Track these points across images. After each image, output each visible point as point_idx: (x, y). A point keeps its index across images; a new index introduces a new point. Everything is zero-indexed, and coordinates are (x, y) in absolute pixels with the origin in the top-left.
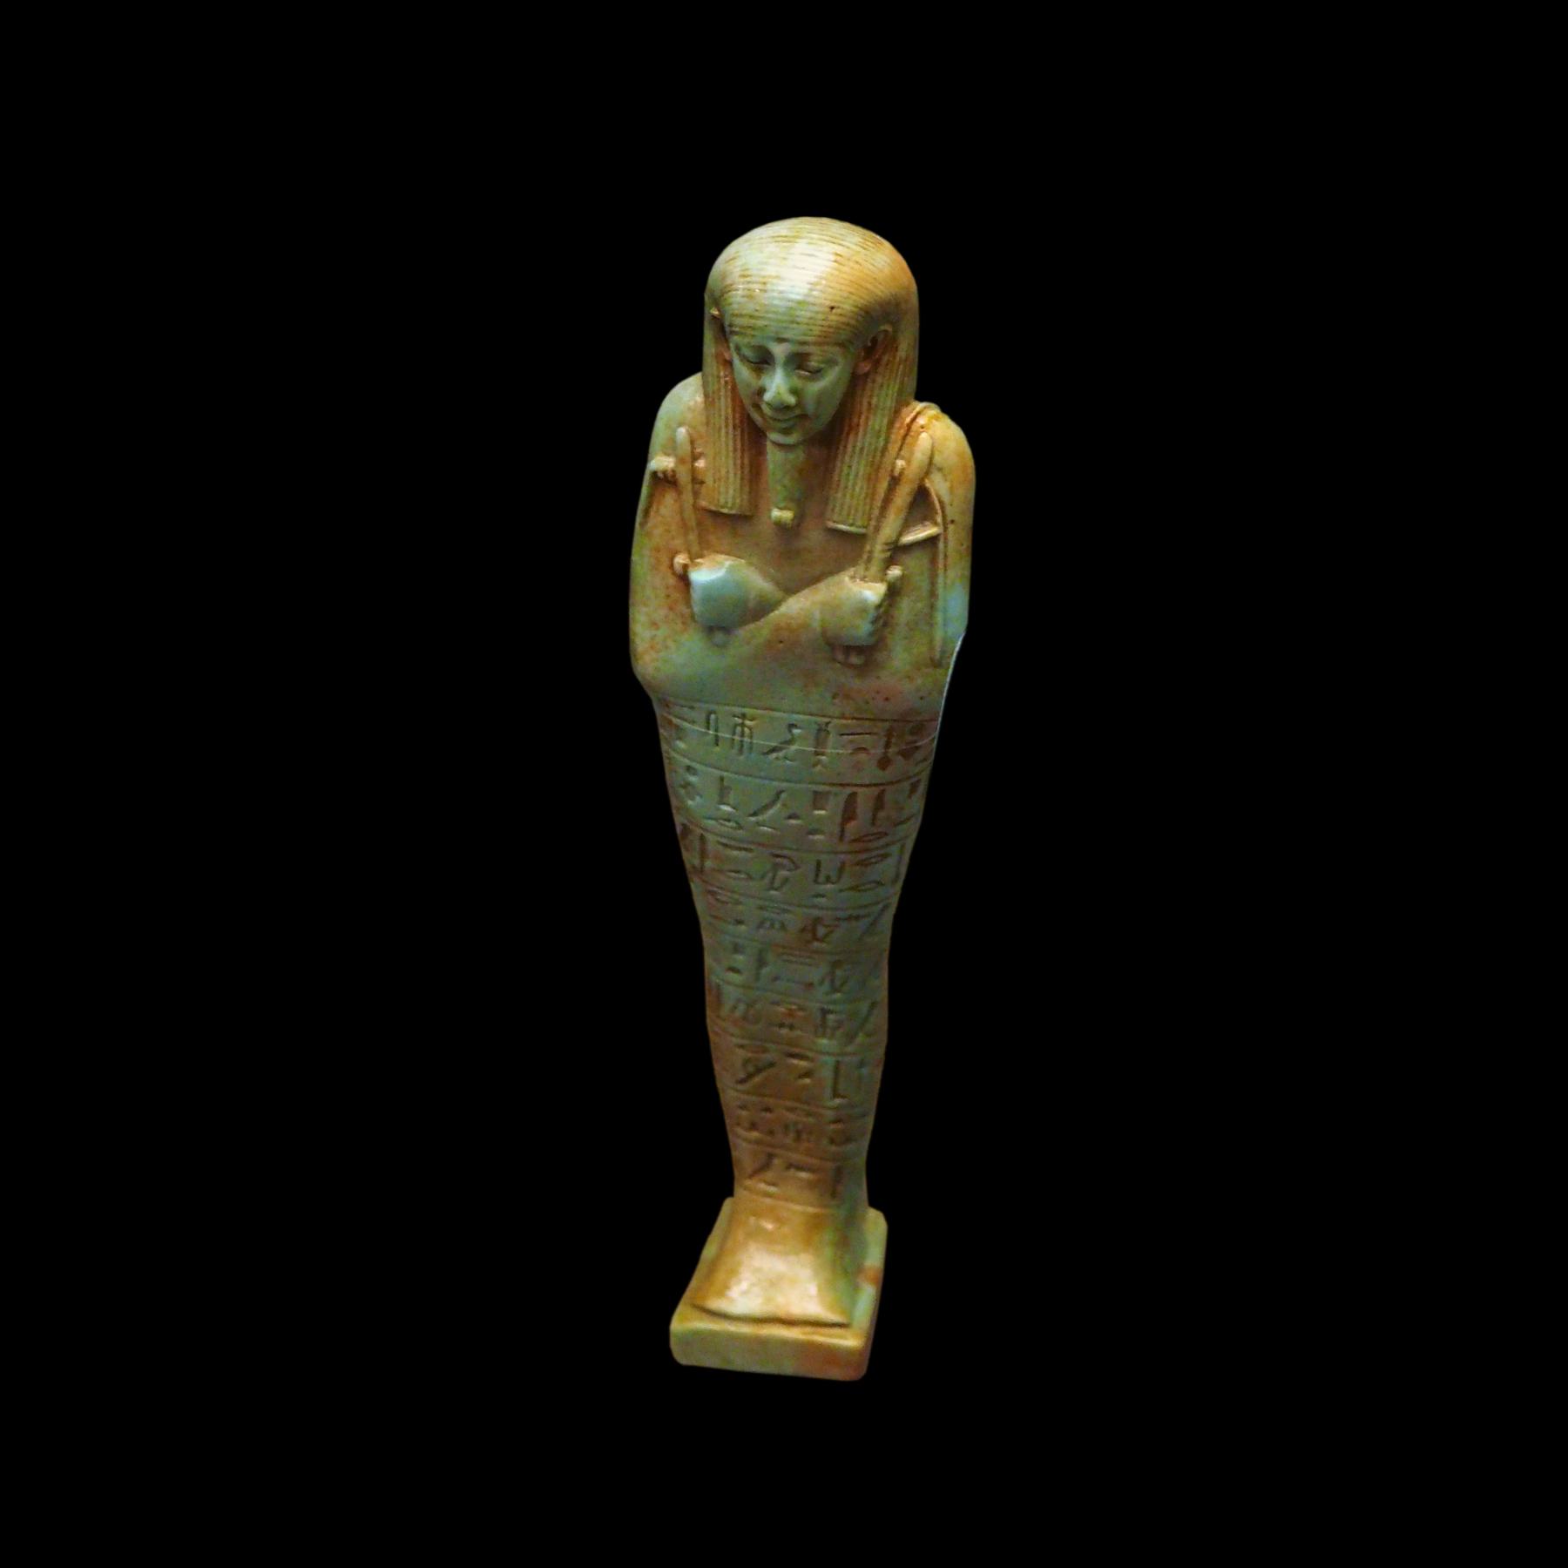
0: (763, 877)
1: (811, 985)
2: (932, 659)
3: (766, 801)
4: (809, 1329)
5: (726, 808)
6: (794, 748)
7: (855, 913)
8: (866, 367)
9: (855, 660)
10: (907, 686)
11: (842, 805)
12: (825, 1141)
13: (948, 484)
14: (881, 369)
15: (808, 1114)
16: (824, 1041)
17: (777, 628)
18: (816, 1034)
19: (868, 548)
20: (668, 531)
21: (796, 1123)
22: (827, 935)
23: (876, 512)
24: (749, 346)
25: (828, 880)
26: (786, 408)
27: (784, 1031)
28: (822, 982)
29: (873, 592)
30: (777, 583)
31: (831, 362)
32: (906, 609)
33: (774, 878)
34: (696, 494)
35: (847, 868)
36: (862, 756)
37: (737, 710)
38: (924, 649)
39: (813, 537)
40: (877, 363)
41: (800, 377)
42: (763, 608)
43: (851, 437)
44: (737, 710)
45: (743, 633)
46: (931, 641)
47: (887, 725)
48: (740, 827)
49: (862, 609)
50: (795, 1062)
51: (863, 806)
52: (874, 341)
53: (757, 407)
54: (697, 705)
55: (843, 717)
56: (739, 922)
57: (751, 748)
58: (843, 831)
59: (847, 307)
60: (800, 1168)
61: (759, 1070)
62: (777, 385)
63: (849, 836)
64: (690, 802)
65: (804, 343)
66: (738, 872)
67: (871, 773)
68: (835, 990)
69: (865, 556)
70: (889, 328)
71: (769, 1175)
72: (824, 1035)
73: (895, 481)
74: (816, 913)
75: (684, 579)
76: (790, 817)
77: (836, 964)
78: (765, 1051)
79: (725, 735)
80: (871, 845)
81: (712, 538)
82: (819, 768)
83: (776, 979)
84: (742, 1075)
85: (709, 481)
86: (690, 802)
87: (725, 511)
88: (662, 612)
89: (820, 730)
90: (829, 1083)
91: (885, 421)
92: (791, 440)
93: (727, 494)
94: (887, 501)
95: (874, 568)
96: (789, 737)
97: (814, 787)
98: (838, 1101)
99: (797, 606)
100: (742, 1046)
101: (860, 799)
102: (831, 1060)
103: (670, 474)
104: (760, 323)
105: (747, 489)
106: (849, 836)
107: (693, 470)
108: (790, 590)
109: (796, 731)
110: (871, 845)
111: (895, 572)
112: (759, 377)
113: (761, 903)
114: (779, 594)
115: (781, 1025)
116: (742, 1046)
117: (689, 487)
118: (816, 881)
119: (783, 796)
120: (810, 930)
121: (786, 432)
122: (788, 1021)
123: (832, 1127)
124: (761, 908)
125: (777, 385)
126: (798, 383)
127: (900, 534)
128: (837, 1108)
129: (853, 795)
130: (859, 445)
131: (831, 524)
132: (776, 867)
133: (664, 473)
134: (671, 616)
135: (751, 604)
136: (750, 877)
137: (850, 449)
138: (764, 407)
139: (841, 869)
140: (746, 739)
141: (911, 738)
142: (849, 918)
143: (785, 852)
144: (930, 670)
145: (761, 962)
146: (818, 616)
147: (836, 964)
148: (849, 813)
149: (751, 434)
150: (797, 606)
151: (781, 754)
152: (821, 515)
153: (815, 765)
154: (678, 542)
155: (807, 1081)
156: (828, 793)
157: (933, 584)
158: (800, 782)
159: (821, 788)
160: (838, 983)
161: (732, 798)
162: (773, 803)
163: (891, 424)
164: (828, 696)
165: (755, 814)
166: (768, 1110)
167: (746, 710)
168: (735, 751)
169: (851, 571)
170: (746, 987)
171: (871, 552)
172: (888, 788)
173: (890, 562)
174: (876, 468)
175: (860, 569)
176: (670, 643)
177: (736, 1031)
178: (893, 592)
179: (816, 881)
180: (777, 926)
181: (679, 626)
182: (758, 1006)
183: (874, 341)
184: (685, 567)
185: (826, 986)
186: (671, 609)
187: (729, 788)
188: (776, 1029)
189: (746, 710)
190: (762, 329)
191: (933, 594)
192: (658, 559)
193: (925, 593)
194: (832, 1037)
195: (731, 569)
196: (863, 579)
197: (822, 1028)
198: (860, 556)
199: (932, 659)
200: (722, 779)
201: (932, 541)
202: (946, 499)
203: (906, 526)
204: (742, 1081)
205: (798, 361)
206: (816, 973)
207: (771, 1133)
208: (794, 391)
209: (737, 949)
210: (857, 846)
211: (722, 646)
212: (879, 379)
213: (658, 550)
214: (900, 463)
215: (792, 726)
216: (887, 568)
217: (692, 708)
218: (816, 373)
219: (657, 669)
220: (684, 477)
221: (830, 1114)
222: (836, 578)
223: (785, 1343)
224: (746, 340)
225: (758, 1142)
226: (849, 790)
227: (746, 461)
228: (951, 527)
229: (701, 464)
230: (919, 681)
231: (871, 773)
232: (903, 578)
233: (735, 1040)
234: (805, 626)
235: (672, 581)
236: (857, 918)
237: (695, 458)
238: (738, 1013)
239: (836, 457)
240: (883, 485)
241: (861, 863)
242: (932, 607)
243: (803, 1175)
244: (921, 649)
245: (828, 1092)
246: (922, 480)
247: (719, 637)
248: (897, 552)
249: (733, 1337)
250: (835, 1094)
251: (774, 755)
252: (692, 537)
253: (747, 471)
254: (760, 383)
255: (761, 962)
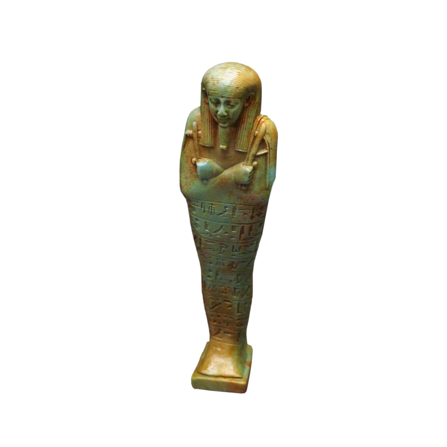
0: (217, 250)
1: (231, 281)
2: (266, 188)
3: (218, 228)
4: (230, 379)
5: (207, 230)
6: (226, 213)
7: (244, 260)
8: (247, 105)
9: (244, 188)
10: (259, 196)
11: (240, 230)
12: (235, 325)
13: (270, 138)
14: (251, 105)
15: (230, 318)
16: (235, 297)
17: (222, 179)
18: (233, 295)
19: (247, 156)
20: (190, 151)
21: (227, 320)
22: (236, 267)
23: (250, 146)
24: (213, 99)
25: (236, 251)
26: (224, 116)
27: (224, 294)
28: (234, 280)
29: (249, 169)
30: (222, 166)
31: (237, 103)
32: (258, 174)
33: (221, 250)
34: (198, 141)
35: (242, 248)
36: (246, 216)
37: (210, 202)
38: (263, 185)
39: (232, 153)
40: (250, 104)
41: (228, 107)
42: (218, 173)
43: (243, 125)
44: (210, 202)
45: (212, 180)
46: (265, 183)
47: (253, 207)
48: (211, 236)
49: (246, 173)
50: (227, 303)
51: (246, 230)
52: (249, 97)
53: (216, 116)
54: (199, 201)
55: (240, 204)
56: (211, 263)
57: (214, 213)
58: (240, 237)
59: (242, 87)
60: (228, 333)
61: (216, 305)
62: (222, 110)
63: (242, 238)
64: (197, 229)
65: (229, 98)
66: (210, 249)
67: (248, 220)
68: (238, 282)
69: (247, 159)
70: (253, 93)
71: (219, 335)
72: (235, 295)
73: (255, 137)
74: (233, 260)
75: (195, 165)
76: (225, 233)
77: (238, 275)
78: (218, 300)
79: (207, 209)
80: (248, 241)
81: (203, 153)
82: (233, 219)
83: (221, 279)
84: (212, 307)
85: (202, 137)
86: (197, 229)
87: (207, 146)
88: (189, 175)
89: (234, 208)
90: (236, 309)
91: (252, 120)
92: (225, 125)
93: (207, 141)
94: (253, 143)
95: (249, 162)
96: (225, 210)
97: (232, 224)
98: (239, 314)
99: (227, 173)
100: (211, 298)
101: (245, 228)
102: (237, 302)
103: (191, 135)
104: (217, 92)
105: (213, 139)
106: (242, 238)
107: (198, 134)
108: (225, 168)
109: (227, 208)
110: (248, 241)
111: (255, 163)
112: (216, 108)
113: (217, 257)
114: (222, 169)
115: (223, 292)
116: (211, 298)
117: (197, 139)
118: (233, 251)
119: (223, 227)
120: (231, 265)
121: (224, 123)
122: (225, 291)
123: (237, 321)
124: (217, 259)
125: (222, 110)
126: (227, 109)
127: (257, 152)
128: (238, 316)
129: (243, 227)
130: (245, 127)
131: (237, 150)
132: (221, 247)
133: (189, 135)
134: (191, 176)
135: (214, 172)
136: (214, 250)
137: (242, 128)
138: (218, 116)
139: (240, 248)
140: (213, 211)
141: (260, 210)
142: (242, 262)
143: (224, 243)
144: (265, 191)
145: (217, 274)
146: (233, 175)
147: (238, 275)
148: (242, 232)
149: (214, 124)
150: (227, 173)
151: (223, 215)
152: (234, 147)
153: (232, 218)
154: (193, 155)
155: (230, 308)
156: (236, 226)
157: (266, 166)
158: (228, 223)
159: (234, 225)
160: (239, 280)
161: (209, 227)
162: (220, 229)
163: (254, 121)
164: (236, 198)
165: (215, 232)
166: (219, 316)
167: (213, 203)
168: (209, 214)
169: (243, 163)
170: (213, 281)
171: (248, 157)
172: (253, 225)
173: (254, 160)
174: (250, 133)
175: (245, 162)
176: (191, 183)
177: (210, 294)
178: (255, 169)
179: (233, 251)
180: (222, 264)
181: (194, 179)
182: (216, 287)
183: (249, 97)
184: (195, 162)
185: (236, 281)
186: (191, 173)
187: (208, 225)
188: (221, 293)
189: (213, 203)
190: (217, 94)
191: (266, 169)
192: (187, 159)
193: (264, 169)
194: (237, 296)
195: (208, 162)
196: (246, 165)
197: (234, 293)
198: (245, 159)
199: (266, 188)
200: (206, 222)
201: (266, 154)
202: (270, 142)
203: (258, 150)
204: (212, 308)
205: (227, 103)
206: (233, 277)
207: (220, 323)
208: (226, 112)
209: (210, 271)
210: (244, 241)
211: (206, 184)
212: (251, 108)
213: (187, 157)
214: (257, 132)
215: (226, 207)
216: (253, 162)
217: (197, 202)
218: (233, 106)
219: (187, 191)
220: (195, 136)
221: (237, 318)
222: (238, 165)
223: (224, 383)
224: (213, 97)
225: (216, 326)
226: (242, 225)
227: (213, 131)
228: (271, 150)
229: (200, 132)
230: (262, 194)
231: (248, 220)
232: (257, 165)
233: (210, 297)
234: (230, 179)
235: (192, 166)
236: (244, 262)
237: (198, 130)
238: (210, 289)
239: (238, 130)
240: (252, 138)
241: (246, 246)
242: (266, 173)
243: (229, 335)
244: (262, 185)
245: (236, 311)
246: (263, 137)
247: (205, 182)
248: (256, 157)
249: (209, 381)
250: (238, 312)
251: (221, 215)
252: (197, 153)
253: (213, 134)
254: (217, 109)
255: (217, 274)
